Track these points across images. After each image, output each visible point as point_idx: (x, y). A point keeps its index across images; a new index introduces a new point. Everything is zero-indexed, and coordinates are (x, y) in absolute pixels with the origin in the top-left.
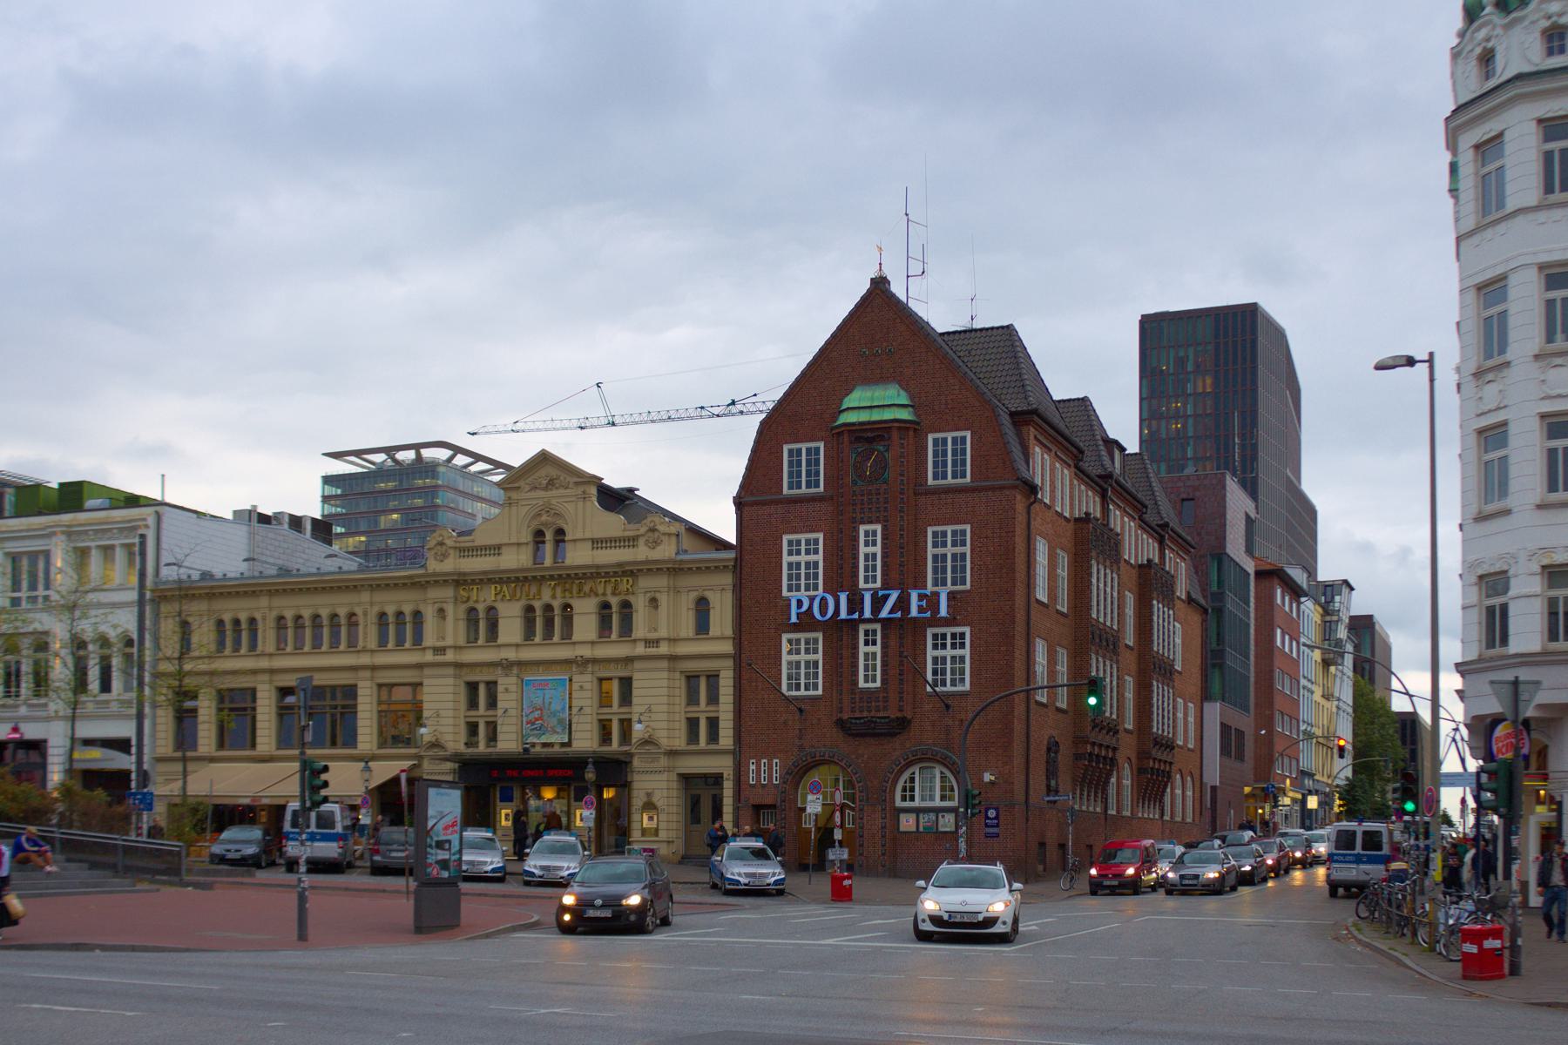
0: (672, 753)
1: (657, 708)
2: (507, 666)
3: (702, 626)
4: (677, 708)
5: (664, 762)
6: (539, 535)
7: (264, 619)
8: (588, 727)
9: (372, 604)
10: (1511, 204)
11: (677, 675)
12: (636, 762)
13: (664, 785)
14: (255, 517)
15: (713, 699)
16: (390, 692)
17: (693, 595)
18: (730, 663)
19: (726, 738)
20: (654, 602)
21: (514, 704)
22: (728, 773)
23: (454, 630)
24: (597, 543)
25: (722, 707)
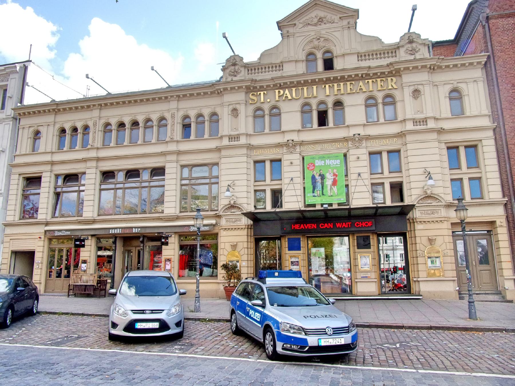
2: (290, 146)
3: (459, 112)
7: (95, 125)
9: (178, 109)
10: (39, 151)
15: (474, 162)
16: (191, 171)
18: (491, 133)
23: (245, 123)
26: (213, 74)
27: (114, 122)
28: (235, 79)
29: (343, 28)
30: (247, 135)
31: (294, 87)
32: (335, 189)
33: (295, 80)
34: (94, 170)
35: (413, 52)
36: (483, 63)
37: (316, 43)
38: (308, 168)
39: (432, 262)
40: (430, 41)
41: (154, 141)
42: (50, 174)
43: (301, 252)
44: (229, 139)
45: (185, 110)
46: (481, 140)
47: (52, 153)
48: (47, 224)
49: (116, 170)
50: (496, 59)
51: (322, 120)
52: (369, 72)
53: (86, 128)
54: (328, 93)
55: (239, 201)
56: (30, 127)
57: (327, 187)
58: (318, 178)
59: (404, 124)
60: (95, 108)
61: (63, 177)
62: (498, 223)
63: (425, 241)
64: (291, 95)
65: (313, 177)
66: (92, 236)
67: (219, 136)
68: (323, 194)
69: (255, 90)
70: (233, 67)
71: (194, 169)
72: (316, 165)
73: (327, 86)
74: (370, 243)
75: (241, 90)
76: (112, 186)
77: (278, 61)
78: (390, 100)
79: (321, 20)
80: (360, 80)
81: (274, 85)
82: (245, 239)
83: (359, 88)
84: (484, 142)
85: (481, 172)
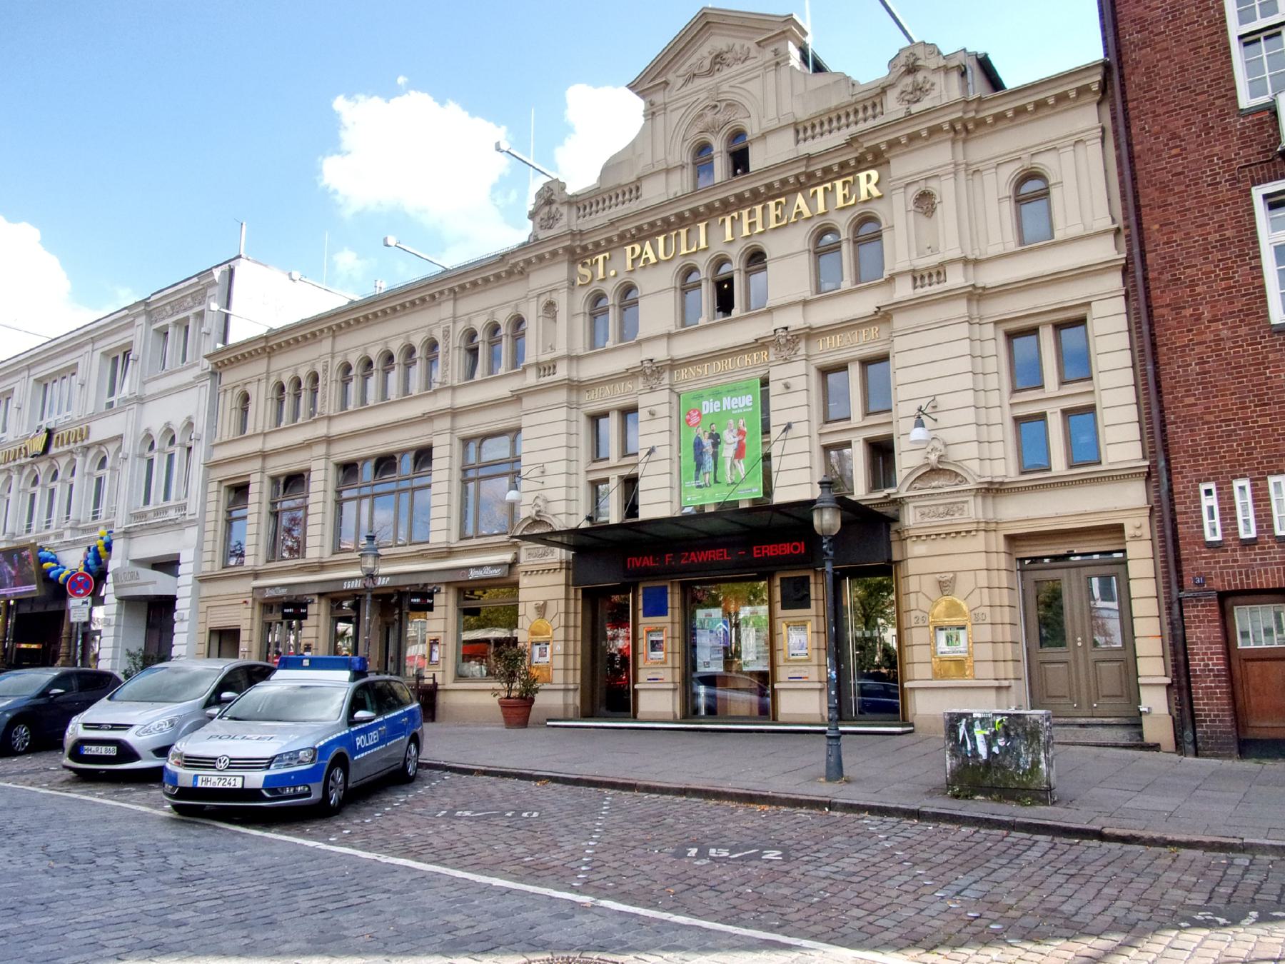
0: (993, 490)
1: (949, 400)
4: (994, 399)
5: (974, 510)
6: (703, 149)
7: (325, 371)
8: (804, 460)
11: (989, 331)
12: (911, 518)
13: (980, 561)
14: (738, 146)
15: (1077, 367)
17: (1009, 172)
18: (1115, 281)
19: (1122, 441)
20: (925, 202)
21: (665, 438)
22: (1138, 526)
24: (801, 129)
25: (1101, 380)
26: (513, 233)
27: (354, 359)
28: (915, 108)
29: (765, 66)
30: (572, 358)
31: (659, 234)
32: (742, 466)
33: (670, 213)
35: (919, 91)
36: (1095, 87)
37: (710, 116)
38: (688, 421)
39: (949, 639)
40: (970, 55)
42: (807, 368)
44: (915, 279)
45: (444, 322)
46: (1089, 304)
47: (265, 435)
48: (256, 575)
49: (397, 452)
50: (1127, 71)
51: (725, 302)
52: (982, 115)
54: (729, 237)
55: (956, 454)
56: (908, 185)
57: (724, 464)
58: (707, 443)
59: (970, 267)
60: (444, 297)
61: (412, 454)
62: (1129, 531)
63: (929, 585)
64: (657, 257)
65: (698, 445)
66: (321, 595)
67: (886, 275)
68: (716, 482)
69: (847, 171)
70: (909, 80)
71: (488, 443)
72: (704, 412)
73: (728, 219)
74: (808, 595)
75: (935, 138)
76: (392, 487)
77: (633, 178)
78: (867, 229)
79: (719, 60)
80: (795, 191)
81: (622, 236)
82: (561, 591)
83: (795, 210)
84: (1097, 309)
85: (1092, 392)
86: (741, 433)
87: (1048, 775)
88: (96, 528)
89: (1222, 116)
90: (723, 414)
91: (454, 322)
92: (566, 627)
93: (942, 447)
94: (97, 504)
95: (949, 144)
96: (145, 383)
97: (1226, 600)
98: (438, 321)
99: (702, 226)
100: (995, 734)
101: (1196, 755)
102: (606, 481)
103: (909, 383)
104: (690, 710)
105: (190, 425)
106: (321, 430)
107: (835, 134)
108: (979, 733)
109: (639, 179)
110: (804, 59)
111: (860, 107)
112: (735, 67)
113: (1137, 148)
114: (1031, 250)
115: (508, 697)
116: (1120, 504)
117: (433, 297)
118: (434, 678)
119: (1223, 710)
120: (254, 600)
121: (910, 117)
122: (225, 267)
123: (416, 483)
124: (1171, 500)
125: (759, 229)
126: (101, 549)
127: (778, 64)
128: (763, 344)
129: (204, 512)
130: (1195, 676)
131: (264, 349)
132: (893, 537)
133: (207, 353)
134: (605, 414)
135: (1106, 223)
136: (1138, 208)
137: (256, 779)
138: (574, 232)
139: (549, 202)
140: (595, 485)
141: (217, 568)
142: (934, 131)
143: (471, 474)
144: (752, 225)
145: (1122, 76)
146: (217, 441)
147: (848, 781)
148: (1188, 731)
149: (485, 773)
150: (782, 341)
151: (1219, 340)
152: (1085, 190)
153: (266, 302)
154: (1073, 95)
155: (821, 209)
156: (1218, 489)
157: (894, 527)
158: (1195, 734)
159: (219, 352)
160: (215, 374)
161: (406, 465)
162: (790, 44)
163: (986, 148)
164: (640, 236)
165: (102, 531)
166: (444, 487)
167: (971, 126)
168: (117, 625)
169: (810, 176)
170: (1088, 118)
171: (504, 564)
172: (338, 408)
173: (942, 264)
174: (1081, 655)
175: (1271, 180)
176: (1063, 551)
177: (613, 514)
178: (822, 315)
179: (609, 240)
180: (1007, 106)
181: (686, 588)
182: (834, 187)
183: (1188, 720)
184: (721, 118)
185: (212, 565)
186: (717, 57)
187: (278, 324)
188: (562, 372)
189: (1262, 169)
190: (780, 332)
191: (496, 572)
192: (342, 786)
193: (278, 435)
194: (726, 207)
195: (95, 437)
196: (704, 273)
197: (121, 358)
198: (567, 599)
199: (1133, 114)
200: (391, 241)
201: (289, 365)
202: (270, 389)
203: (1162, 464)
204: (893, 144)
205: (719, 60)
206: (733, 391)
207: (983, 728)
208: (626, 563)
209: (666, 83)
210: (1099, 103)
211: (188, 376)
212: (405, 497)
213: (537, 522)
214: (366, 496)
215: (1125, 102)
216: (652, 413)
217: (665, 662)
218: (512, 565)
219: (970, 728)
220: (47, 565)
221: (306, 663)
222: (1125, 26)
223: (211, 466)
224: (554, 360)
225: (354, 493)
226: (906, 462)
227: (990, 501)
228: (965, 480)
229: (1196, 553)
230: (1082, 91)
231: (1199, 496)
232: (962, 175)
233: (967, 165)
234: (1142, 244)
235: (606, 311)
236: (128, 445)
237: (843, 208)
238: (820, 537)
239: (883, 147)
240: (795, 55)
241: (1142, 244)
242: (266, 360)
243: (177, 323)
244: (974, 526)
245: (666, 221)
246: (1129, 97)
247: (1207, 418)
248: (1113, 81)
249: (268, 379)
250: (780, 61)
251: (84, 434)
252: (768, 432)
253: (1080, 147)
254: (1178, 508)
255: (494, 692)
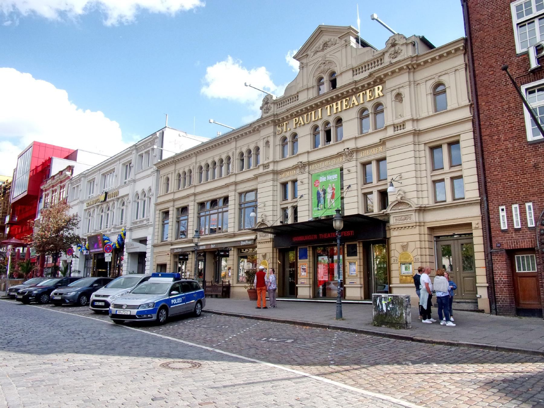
0: (422, 210)
1: (407, 174)
5: (415, 218)
7: (233, 155)
11: (422, 147)
12: (392, 221)
14: (333, 78)
15: (455, 163)
17: (431, 83)
18: (469, 126)
19: (471, 189)
20: (399, 97)
22: (477, 223)
24: (355, 71)
25: (465, 166)
27: (203, 164)
29: (342, 46)
30: (275, 162)
31: (305, 113)
32: (333, 201)
33: (308, 105)
34: (233, 193)
35: (396, 53)
36: (461, 48)
39: (406, 269)
41: (371, 131)
43: (358, 257)
45: (231, 150)
46: (459, 135)
48: (172, 244)
50: (473, 41)
53: (229, 158)
54: (329, 114)
55: (409, 196)
62: (474, 226)
65: (318, 194)
68: (325, 208)
70: (393, 49)
71: (248, 194)
74: (357, 251)
75: (402, 72)
77: (296, 92)
78: (378, 108)
79: (325, 45)
80: (352, 95)
84: (462, 138)
85: (461, 170)
86: (333, 189)
87: (406, 318)
88: (121, 228)
89: (510, 57)
90: (328, 181)
91: (236, 150)
92: (273, 263)
93: (403, 194)
94: (122, 219)
95: (407, 74)
96: (136, 175)
97: (511, 254)
98: (231, 150)
99: (320, 110)
100: (389, 303)
101: (496, 314)
102: (371, 193)
103: (392, 169)
104: (316, 295)
105: (150, 190)
106: (192, 191)
107: (364, 73)
108: (384, 302)
109: (298, 93)
110: (357, 41)
111: (376, 60)
112: (332, 47)
113: (477, 72)
114: (441, 113)
115: (251, 289)
116: (471, 215)
117: (228, 140)
118: (229, 282)
119: (507, 297)
120: (171, 253)
121: (391, 64)
122: (161, 131)
123: (225, 209)
124: (488, 213)
125: (339, 110)
126: (122, 235)
127: (346, 45)
128: (340, 155)
129: (155, 221)
130: (496, 283)
131: (173, 161)
132: (387, 228)
133: (155, 163)
134: (370, 163)
135: (467, 102)
136: (477, 96)
137: (134, 312)
138: (277, 114)
139: (267, 103)
140: (365, 195)
141: (159, 242)
142: (401, 69)
143: (243, 206)
144: (337, 109)
145: (471, 43)
146: (159, 195)
147: (343, 320)
148: (495, 306)
149: (225, 314)
150: (347, 153)
151: (507, 149)
152: (458, 91)
153: (175, 144)
154: (453, 52)
155: (362, 102)
156: (506, 208)
157: (387, 225)
158: (496, 306)
159: (159, 163)
160: (158, 171)
161: (221, 203)
162: (351, 37)
163: (422, 74)
164: (298, 114)
165: (123, 228)
166: (233, 211)
167: (415, 66)
168: (128, 263)
169: (357, 89)
170: (460, 61)
171: (252, 240)
172: (198, 182)
173: (404, 122)
174: (458, 274)
175: (528, 83)
176: (451, 234)
177: (290, 221)
178: (362, 143)
179: (287, 117)
180: (436, 55)
181: (314, 249)
182: (366, 93)
183: (494, 301)
184: (327, 67)
185: (158, 241)
186: (325, 44)
187: (179, 152)
188: (271, 168)
189: (525, 78)
190: (346, 150)
191: (250, 243)
192: (165, 316)
193: (284, 162)
194: (328, 102)
195: (120, 195)
196: (321, 128)
197: (128, 166)
198: (273, 253)
199: (475, 58)
200: (212, 121)
201: (183, 167)
202: (428, 88)
203: (485, 198)
204: (386, 75)
205: (325, 45)
206: (331, 173)
207: (385, 301)
208: (294, 238)
209: (307, 55)
210: (464, 54)
211: (149, 172)
212: (208, 217)
213: (263, 224)
214: (208, 215)
215: (472, 54)
216: (302, 182)
217: (357, 276)
218: (255, 240)
219: (381, 301)
220: (106, 241)
221: (160, 275)
222: (473, 22)
223: (157, 205)
224: (268, 163)
225: (216, 211)
226: (391, 199)
227: (421, 214)
228: (410, 206)
229: (498, 234)
230: (457, 50)
231: (499, 211)
232: (412, 85)
233: (414, 81)
234: (478, 111)
235: (287, 144)
236: (130, 197)
237: (369, 101)
238: (336, 230)
239: (382, 76)
240: (353, 40)
241: (478, 111)
242: (174, 166)
243: (146, 152)
244: (414, 224)
245: (306, 108)
246: (474, 51)
247: (502, 180)
248: (468, 45)
249: (175, 172)
250: (347, 44)
251: (117, 194)
252: (343, 189)
253: (457, 72)
254: (491, 216)
255: (245, 287)
